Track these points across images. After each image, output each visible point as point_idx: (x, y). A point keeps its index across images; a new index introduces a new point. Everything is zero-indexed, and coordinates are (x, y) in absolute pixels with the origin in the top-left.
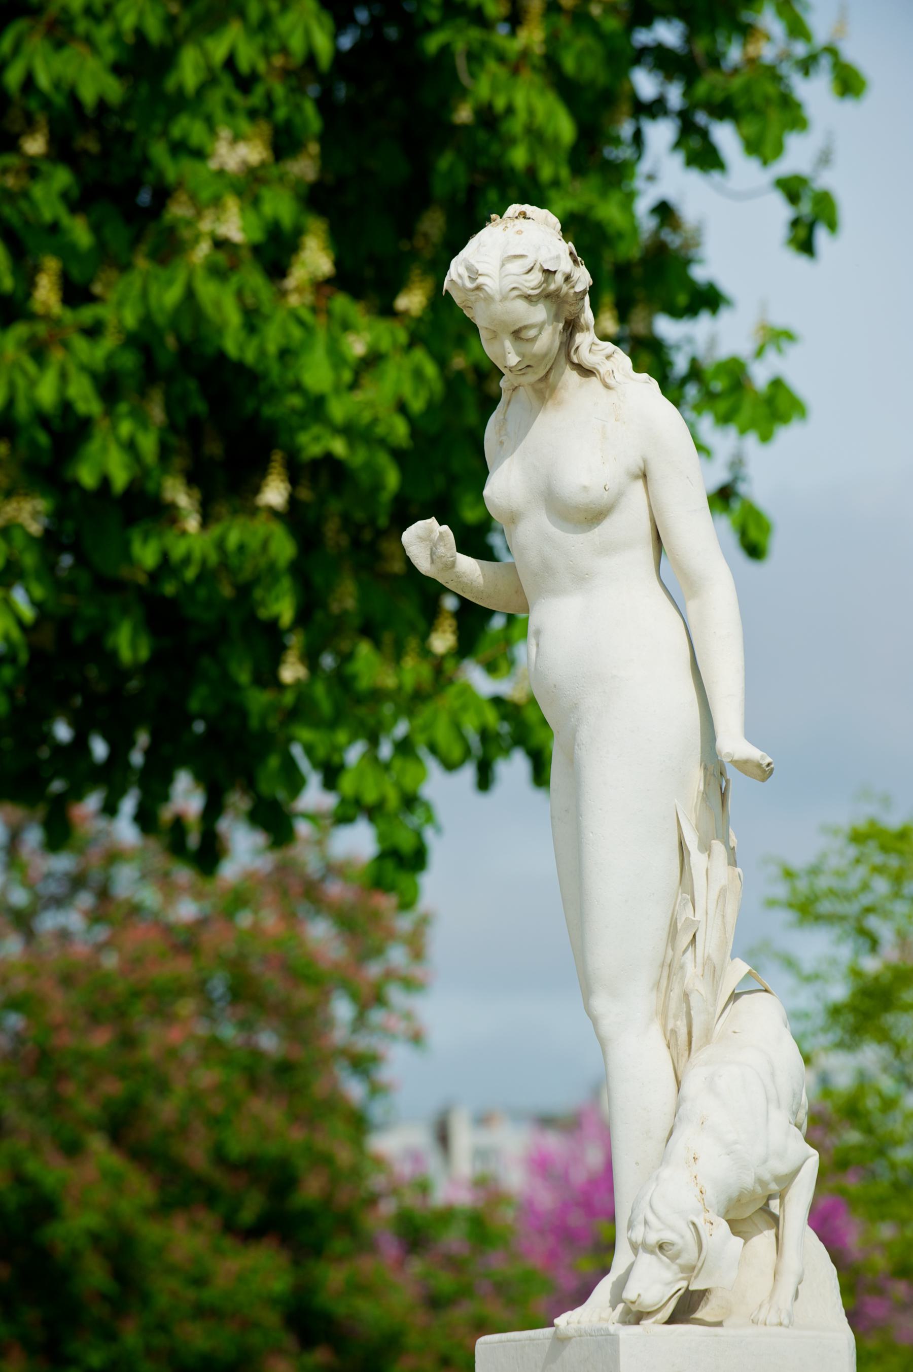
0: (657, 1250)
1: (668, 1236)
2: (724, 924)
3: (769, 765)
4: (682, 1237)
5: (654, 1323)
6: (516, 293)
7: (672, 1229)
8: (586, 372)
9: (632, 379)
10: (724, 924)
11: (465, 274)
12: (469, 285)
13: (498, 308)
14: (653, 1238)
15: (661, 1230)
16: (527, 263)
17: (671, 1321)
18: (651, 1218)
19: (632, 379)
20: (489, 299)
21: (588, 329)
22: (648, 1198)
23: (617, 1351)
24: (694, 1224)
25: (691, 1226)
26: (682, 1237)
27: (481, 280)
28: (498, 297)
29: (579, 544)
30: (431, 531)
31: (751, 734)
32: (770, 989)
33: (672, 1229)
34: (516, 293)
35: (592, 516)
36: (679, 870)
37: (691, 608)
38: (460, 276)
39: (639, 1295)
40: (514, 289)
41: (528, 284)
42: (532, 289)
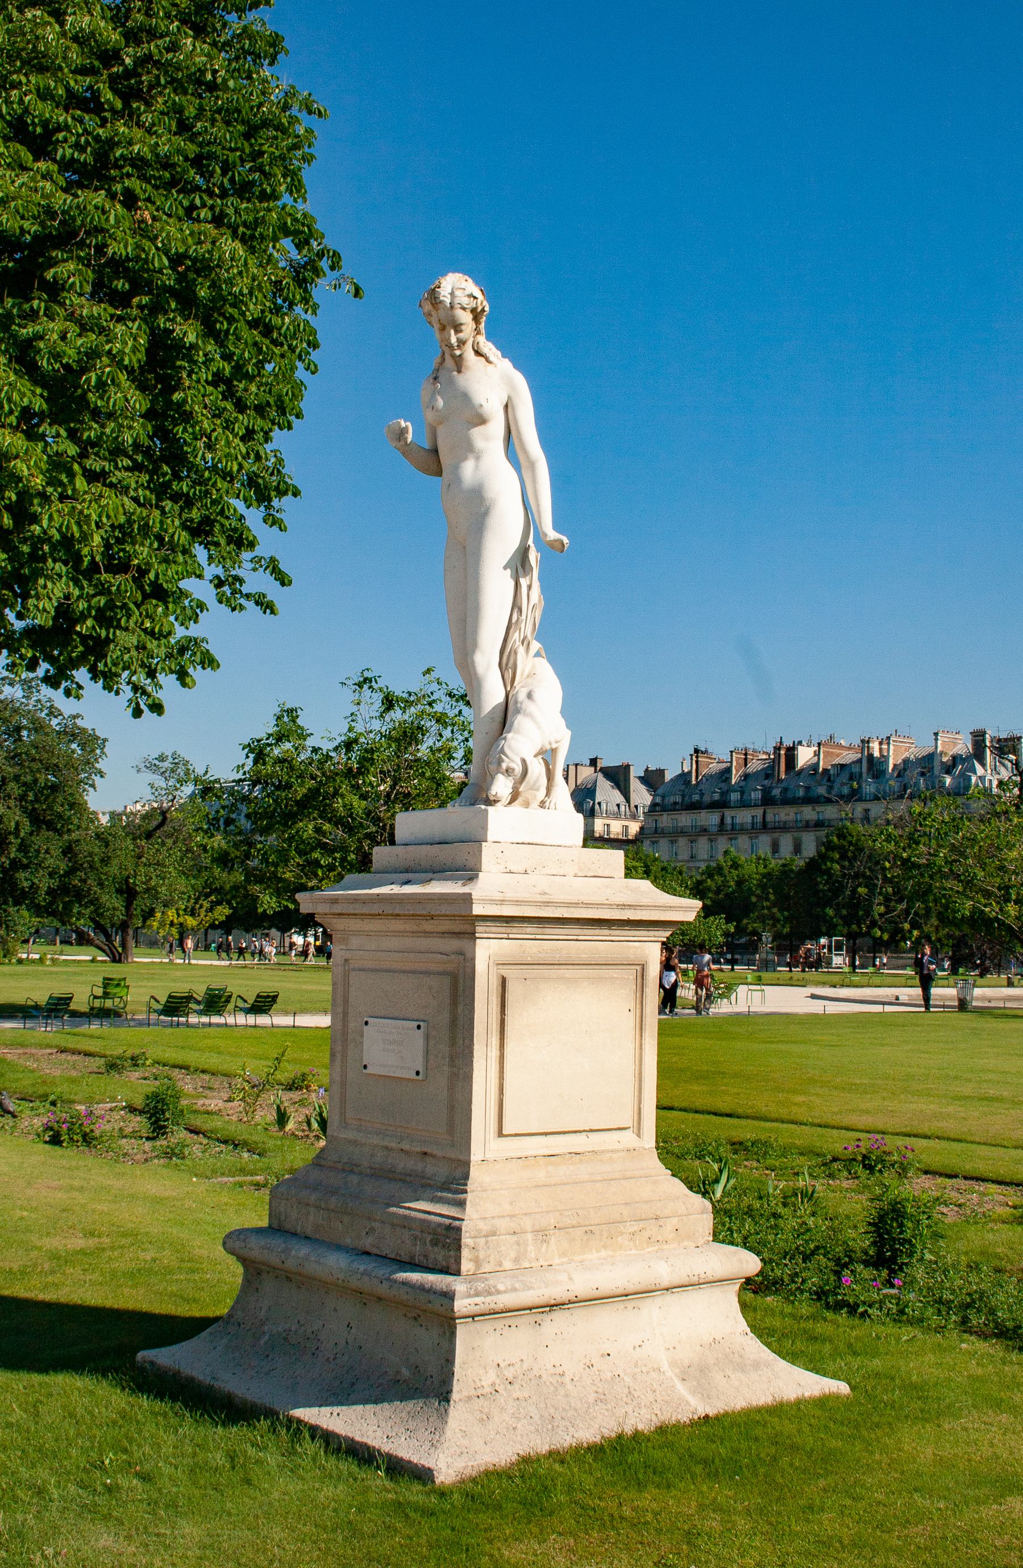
8: (478, 353)
31: (556, 527)
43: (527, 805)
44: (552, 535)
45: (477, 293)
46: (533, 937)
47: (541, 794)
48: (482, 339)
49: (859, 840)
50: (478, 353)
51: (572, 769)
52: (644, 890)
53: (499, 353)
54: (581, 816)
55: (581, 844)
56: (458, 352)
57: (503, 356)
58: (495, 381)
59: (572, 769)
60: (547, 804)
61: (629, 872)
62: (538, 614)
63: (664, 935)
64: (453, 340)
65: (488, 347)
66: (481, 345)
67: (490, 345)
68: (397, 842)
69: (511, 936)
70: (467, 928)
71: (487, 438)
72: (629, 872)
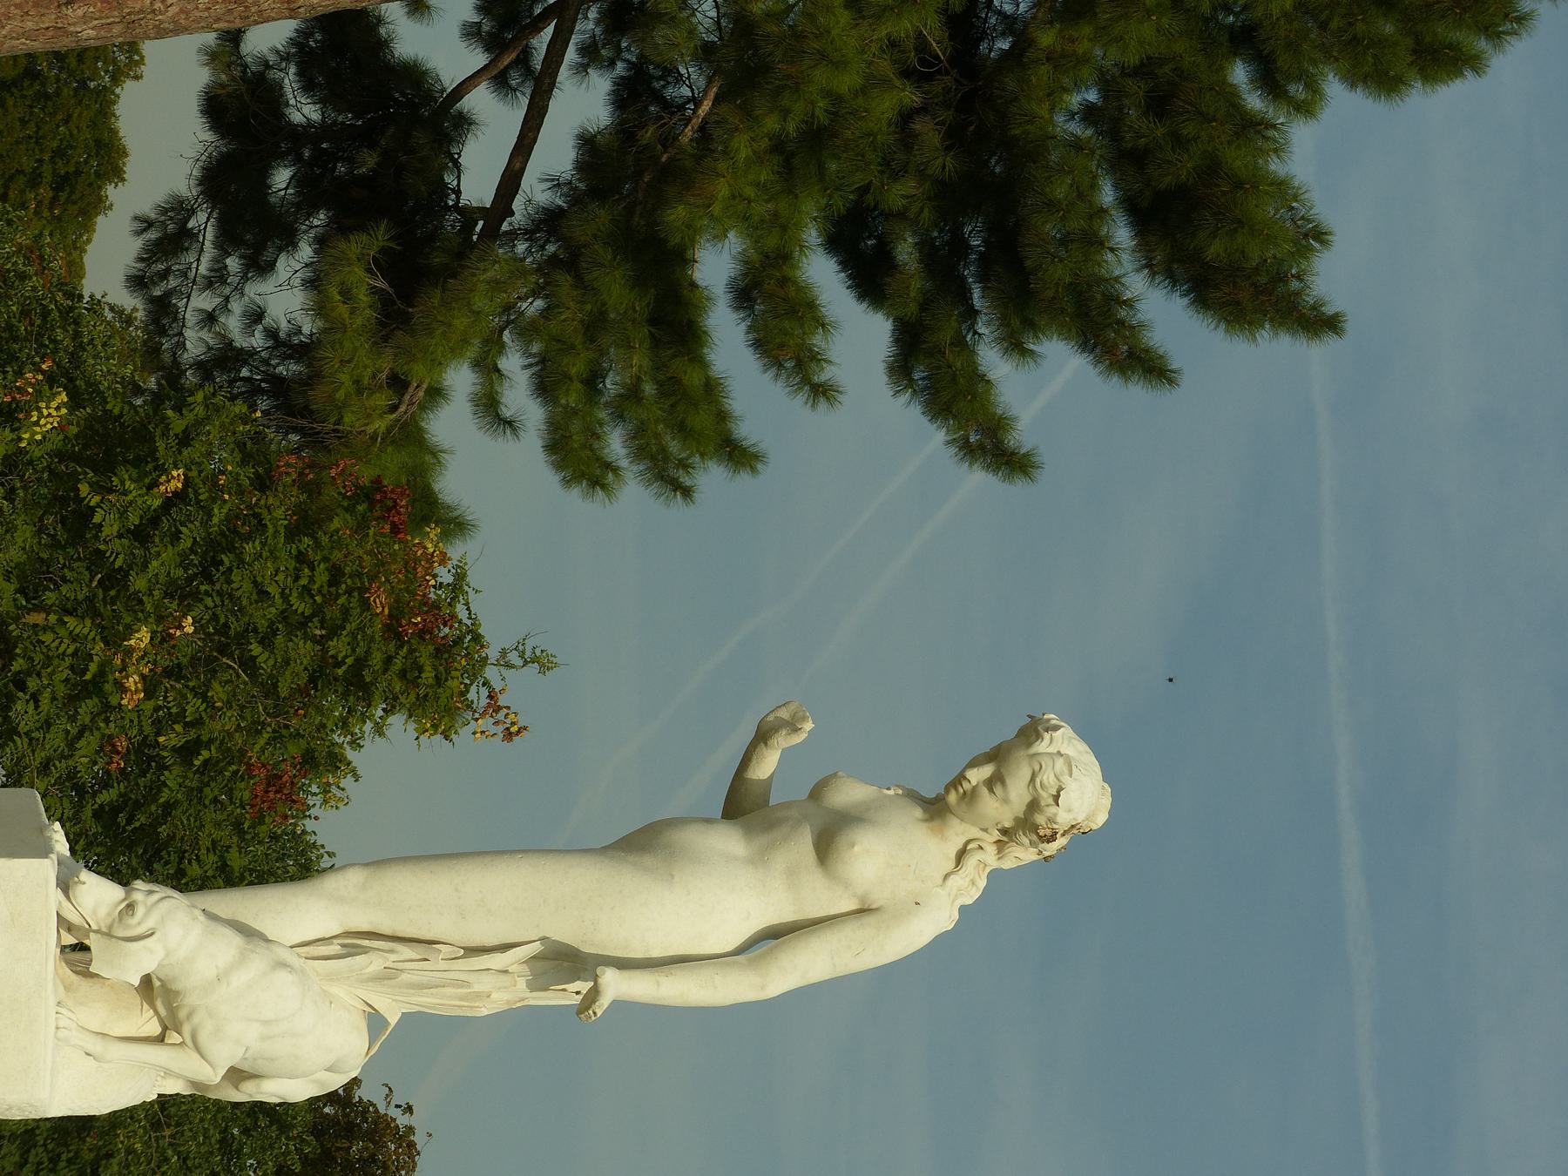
1: (140, 911)
6: (1037, 768)
8: (961, 855)
16: (1065, 779)
18: (156, 897)
34: (1037, 768)
50: (961, 855)
58: (914, 885)
71: (792, 873)
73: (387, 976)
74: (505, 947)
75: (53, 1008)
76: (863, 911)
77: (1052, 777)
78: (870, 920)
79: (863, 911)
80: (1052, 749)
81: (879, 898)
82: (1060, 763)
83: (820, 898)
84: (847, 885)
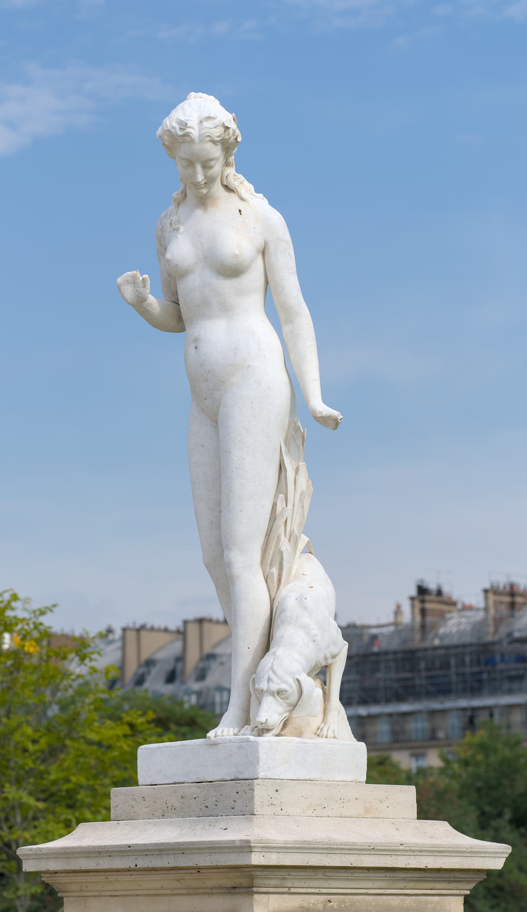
0: (276, 695)
1: (283, 686)
2: (303, 511)
3: (341, 419)
4: (291, 687)
5: (272, 735)
6: (208, 139)
7: (286, 682)
8: (228, 188)
9: (256, 197)
10: (303, 511)
11: (177, 127)
12: (180, 133)
13: (197, 147)
14: (274, 687)
15: (280, 683)
16: (216, 122)
17: (278, 735)
18: (273, 676)
19: (256, 197)
20: (192, 141)
21: (232, 166)
22: (269, 665)
23: (257, 751)
24: (298, 680)
25: (296, 682)
26: (291, 687)
27: (188, 130)
28: (197, 140)
29: (227, 286)
30: (134, 277)
31: (326, 401)
32: (313, 552)
33: (286, 682)
34: (208, 139)
35: (232, 271)
36: (277, 478)
37: (286, 329)
38: (174, 128)
39: (267, 720)
40: (208, 136)
41: (215, 134)
42: (218, 137)
43: (300, 734)
44: (321, 408)
45: (233, 126)
46: (317, 891)
47: (317, 721)
48: (231, 171)
49: (37, 626)
50: (228, 188)
51: (131, 636)
52: (441, 834)
53: (251, 187)
54: (363, 746)
55: (364, 778)
56: (204, 191)
57: (257, 191)
58: (245, 221)
59: (131, 636)
60: (325, 732)
61: (423, 814)
62: (307, 504)
63: (466, 889)
64: (200, 178)
65: (245, 187)
66: (231, 178)
67: (241, 177)
68: (139, 784)
69: (292, 890)
70: (244, 882)
71: (242, 293)
72: (423, 814)
73: (293, 539)
74: (281, 468)
75: (324, 740)
76: (264, 252)
77: (215, 130)
78: (271, 248)
79: (264, 252)
80: (196, 127)
81: (259, 243)
82: (206, 124)
83: (254, 277)
84: (252, 261)
